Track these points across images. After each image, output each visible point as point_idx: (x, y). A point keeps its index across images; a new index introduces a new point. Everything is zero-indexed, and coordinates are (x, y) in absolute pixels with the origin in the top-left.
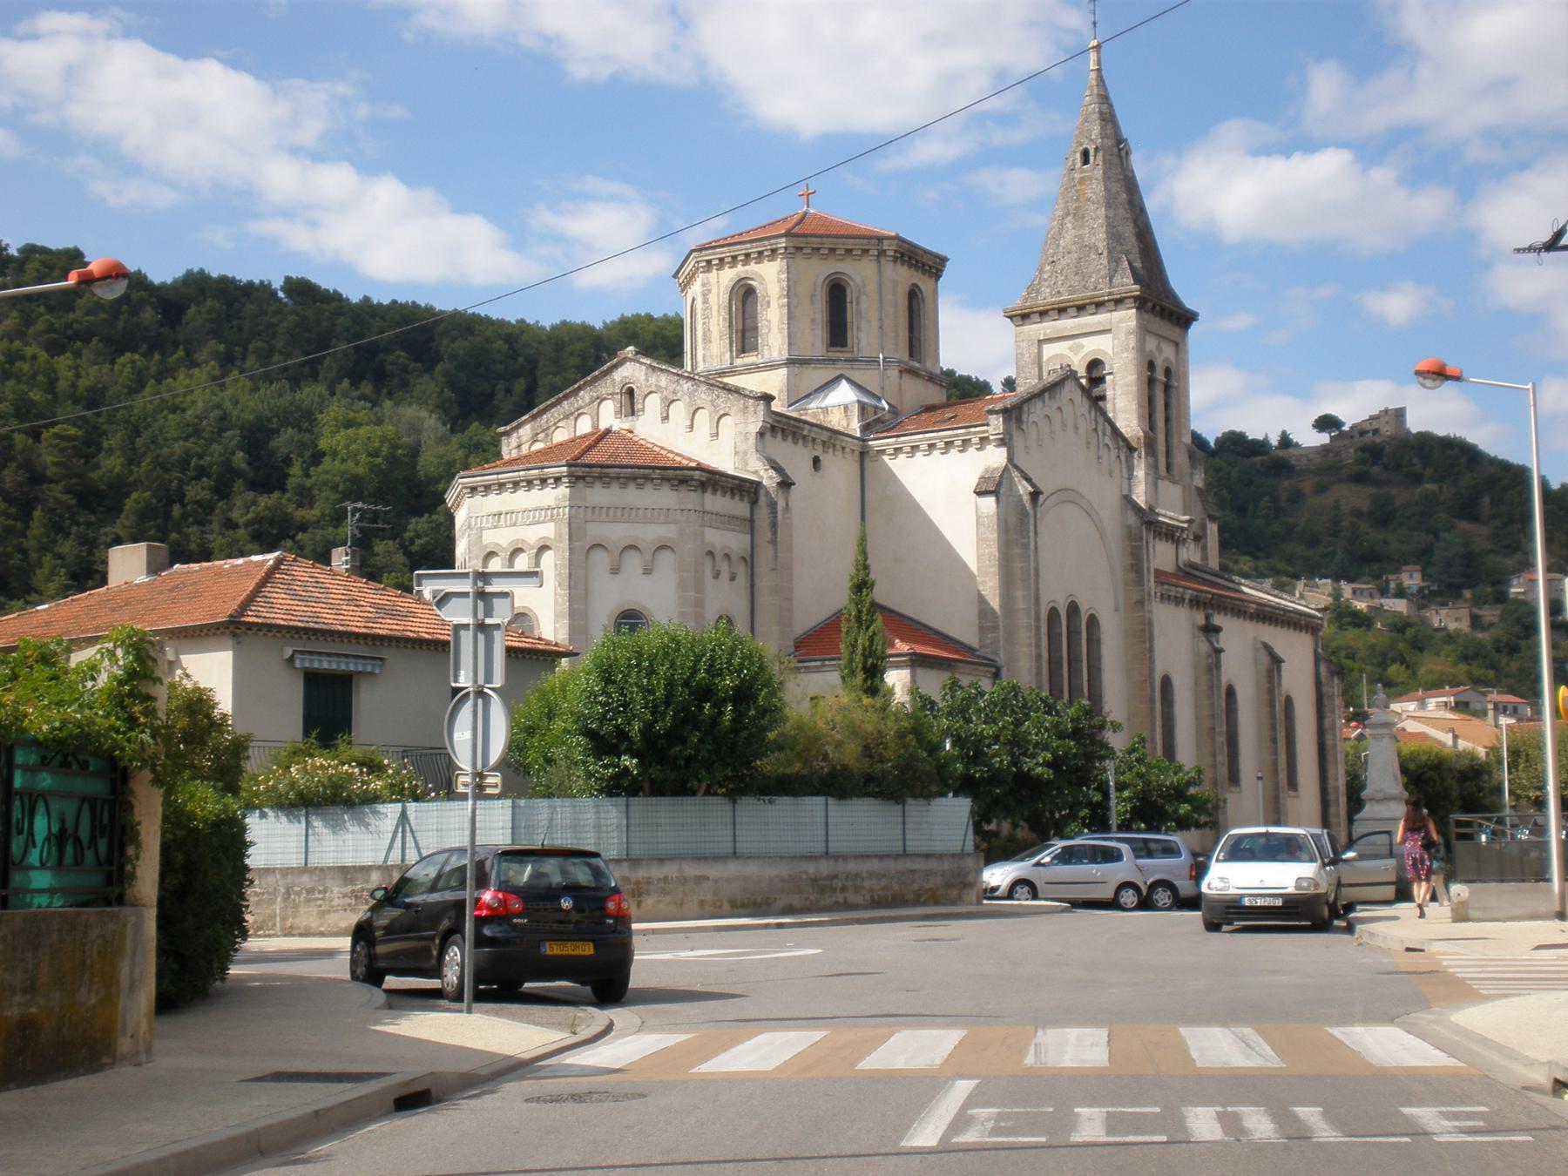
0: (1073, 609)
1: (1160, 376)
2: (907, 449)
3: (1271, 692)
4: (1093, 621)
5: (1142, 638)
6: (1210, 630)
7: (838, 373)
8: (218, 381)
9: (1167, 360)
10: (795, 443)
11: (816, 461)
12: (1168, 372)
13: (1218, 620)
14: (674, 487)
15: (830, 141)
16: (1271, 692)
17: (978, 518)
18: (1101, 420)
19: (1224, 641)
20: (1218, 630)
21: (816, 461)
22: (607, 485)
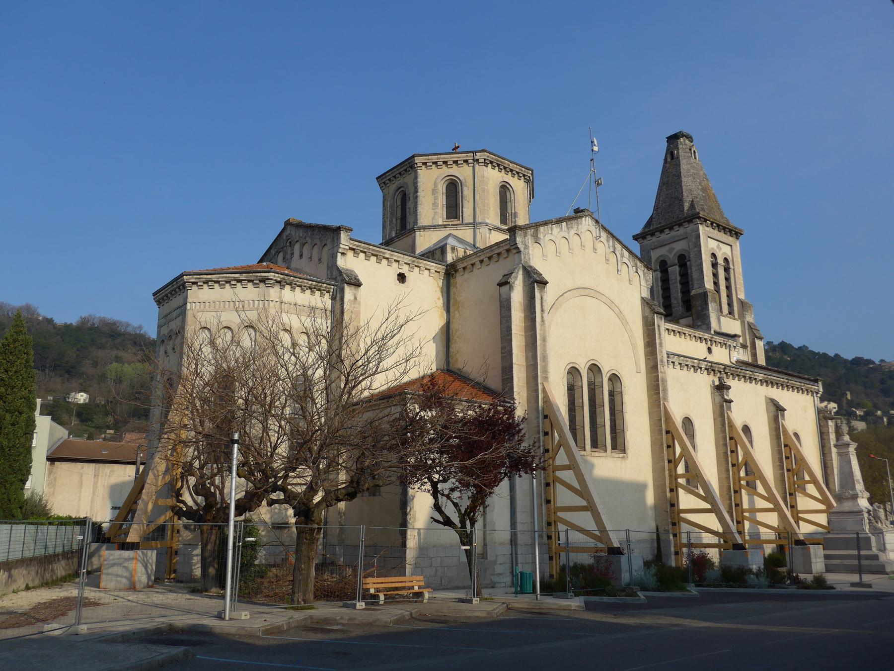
0: (595, 369)
1: (720, 261)
2: (469, 266)
3: (777, 429)
4: (615, 378)
5: (656, 389)
6: (721, 388)
7: (448, 233)
8: (596, 403)
9: (725, 253)
10: (379, 262)
11: (402, 278)
12: (726, 260)
13: (730, 382)
14: (256, 286)
15: (867, 360)
16: (777, 429)
17: (501, 302)
18: (618, 246)
19: (731, 395)
20: (729, 388)
21: (402, 278)
22: (211, 287)
